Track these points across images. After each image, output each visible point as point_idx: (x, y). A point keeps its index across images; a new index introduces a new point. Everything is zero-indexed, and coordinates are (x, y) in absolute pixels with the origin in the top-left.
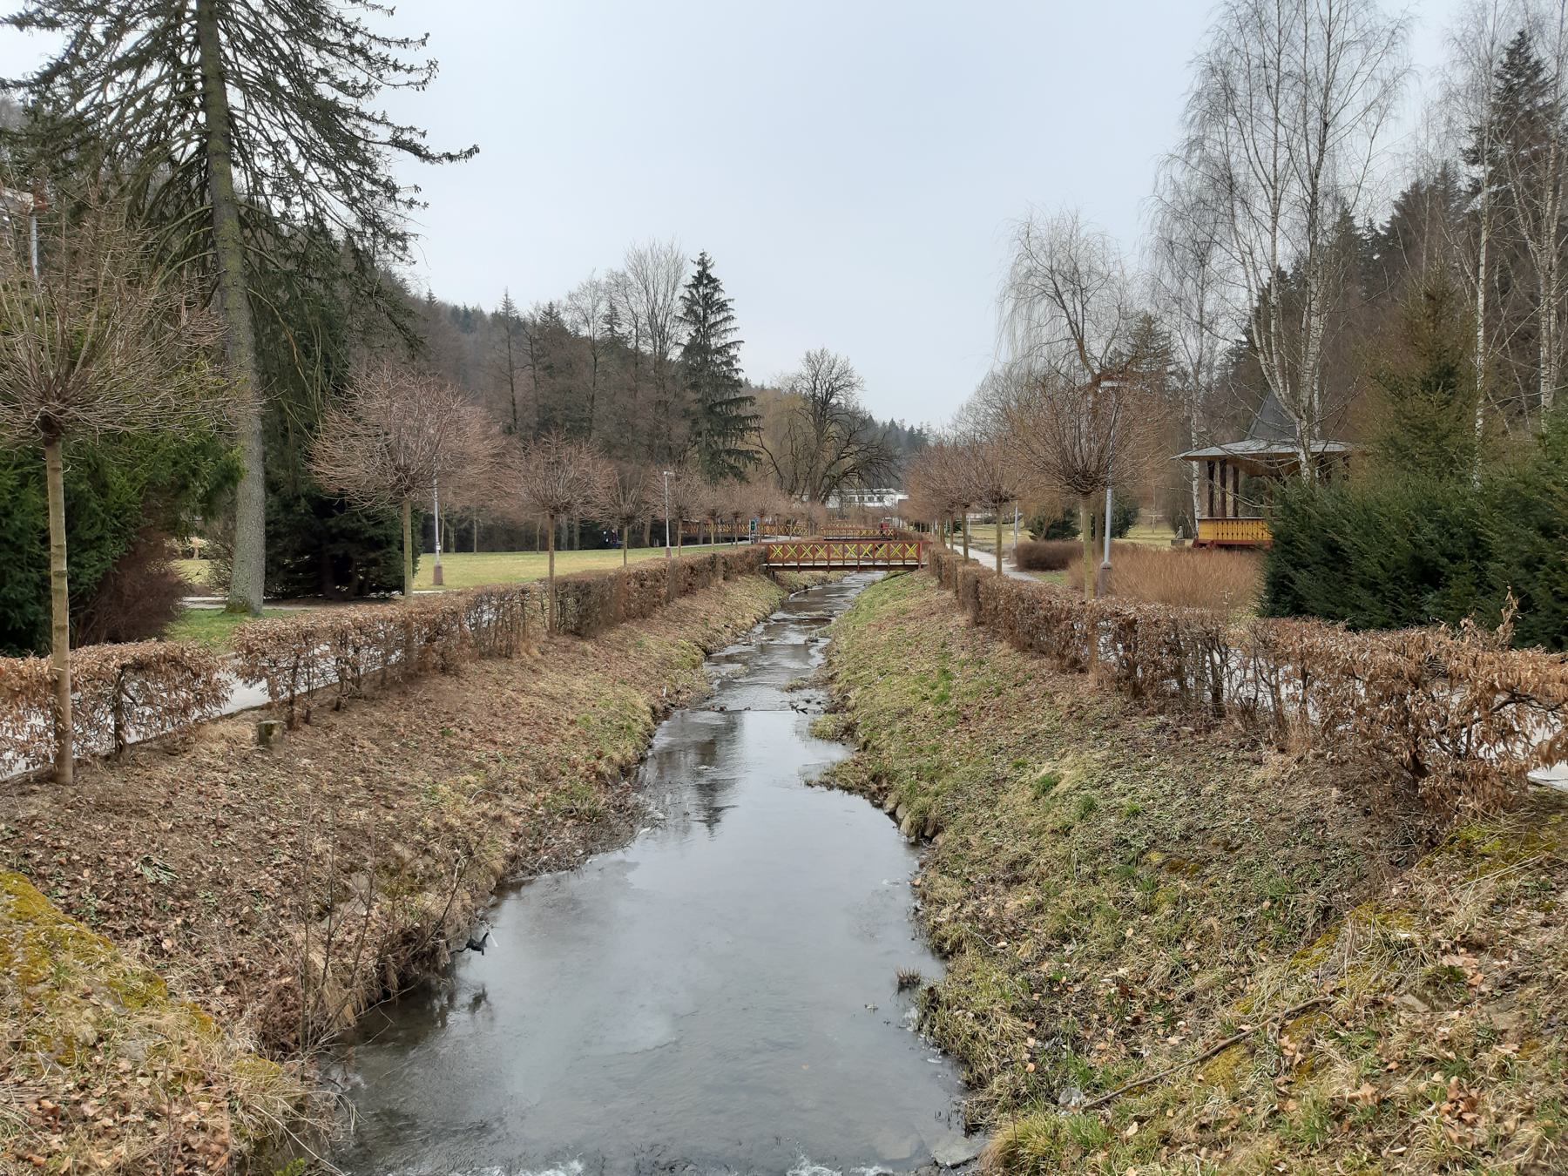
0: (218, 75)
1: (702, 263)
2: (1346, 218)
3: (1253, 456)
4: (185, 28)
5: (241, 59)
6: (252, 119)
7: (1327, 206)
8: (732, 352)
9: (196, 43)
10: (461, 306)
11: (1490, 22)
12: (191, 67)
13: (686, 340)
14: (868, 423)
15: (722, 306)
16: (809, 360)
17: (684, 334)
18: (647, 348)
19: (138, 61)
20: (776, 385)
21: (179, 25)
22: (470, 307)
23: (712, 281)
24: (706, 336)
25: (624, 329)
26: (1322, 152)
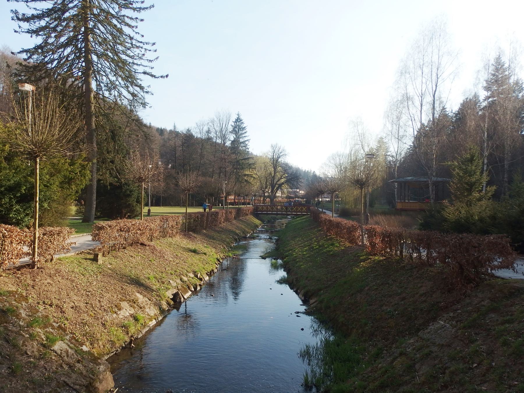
0: (88, 51)
1: (238, 115)
2: (444, 108)
3: (414, 181)
4: (80, 37)
5: (97, 47)
6: (100, 66)
7: (437, 105)
8: (247, 143)
9: (83, 41)
10: (160, 128)
11: (237, 231)
12: (81, 48)
13: (232, 139)
14: (290, 168)
15: (244, 128)
16: (272, 146)
17: (232, 137)
18: (219, 141)
19: (65, 46)
20: (261, 155)
21: (78, 35)
22: (162, 128)
23: (241, 120)
24: (239, 138)
25: (212, 135)
26: (436, 86)
